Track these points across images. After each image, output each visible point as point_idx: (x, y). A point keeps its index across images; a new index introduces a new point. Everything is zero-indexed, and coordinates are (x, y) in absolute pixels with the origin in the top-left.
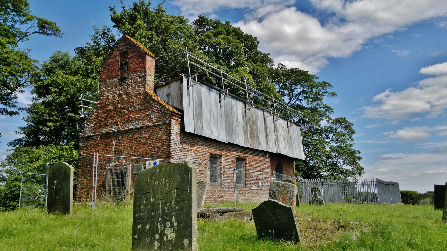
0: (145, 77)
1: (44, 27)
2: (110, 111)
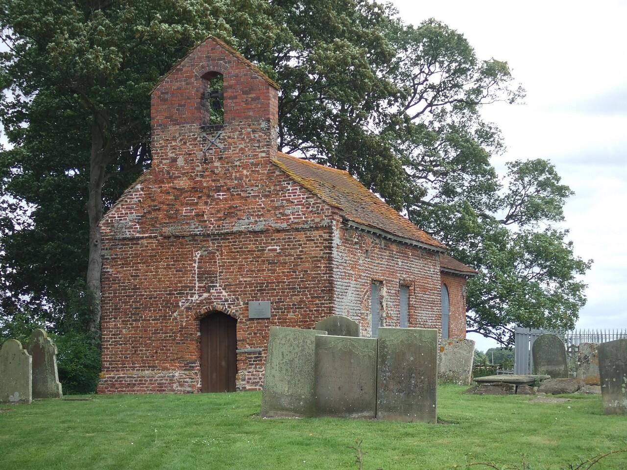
2: (182, 191)
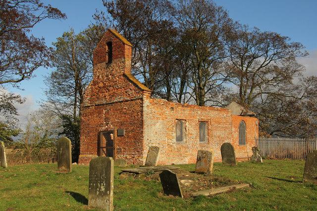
0: (124, 62)
1: (54, 12)
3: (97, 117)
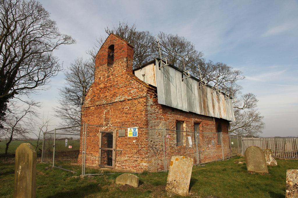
3: (97, 117)
